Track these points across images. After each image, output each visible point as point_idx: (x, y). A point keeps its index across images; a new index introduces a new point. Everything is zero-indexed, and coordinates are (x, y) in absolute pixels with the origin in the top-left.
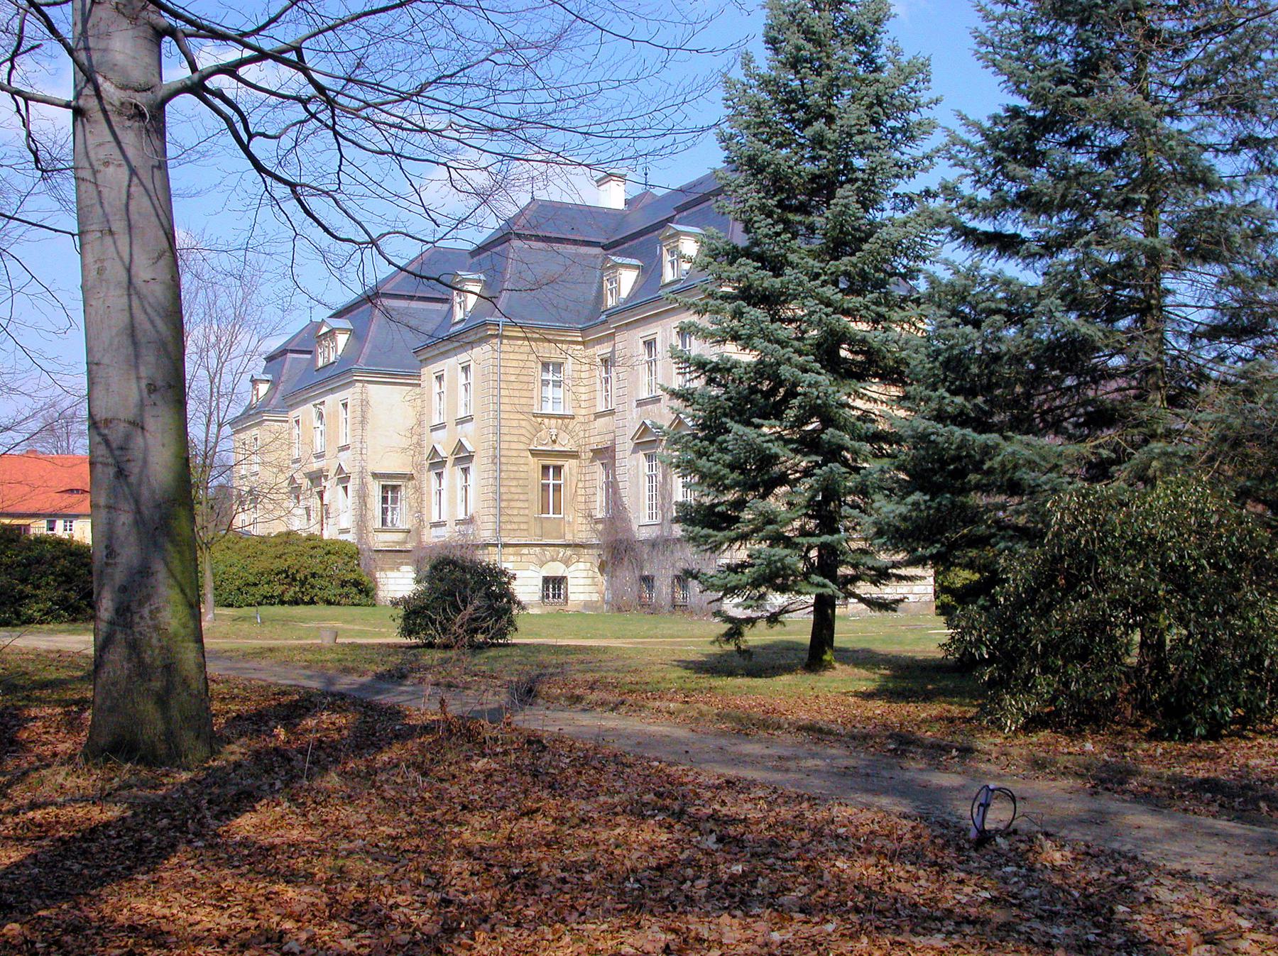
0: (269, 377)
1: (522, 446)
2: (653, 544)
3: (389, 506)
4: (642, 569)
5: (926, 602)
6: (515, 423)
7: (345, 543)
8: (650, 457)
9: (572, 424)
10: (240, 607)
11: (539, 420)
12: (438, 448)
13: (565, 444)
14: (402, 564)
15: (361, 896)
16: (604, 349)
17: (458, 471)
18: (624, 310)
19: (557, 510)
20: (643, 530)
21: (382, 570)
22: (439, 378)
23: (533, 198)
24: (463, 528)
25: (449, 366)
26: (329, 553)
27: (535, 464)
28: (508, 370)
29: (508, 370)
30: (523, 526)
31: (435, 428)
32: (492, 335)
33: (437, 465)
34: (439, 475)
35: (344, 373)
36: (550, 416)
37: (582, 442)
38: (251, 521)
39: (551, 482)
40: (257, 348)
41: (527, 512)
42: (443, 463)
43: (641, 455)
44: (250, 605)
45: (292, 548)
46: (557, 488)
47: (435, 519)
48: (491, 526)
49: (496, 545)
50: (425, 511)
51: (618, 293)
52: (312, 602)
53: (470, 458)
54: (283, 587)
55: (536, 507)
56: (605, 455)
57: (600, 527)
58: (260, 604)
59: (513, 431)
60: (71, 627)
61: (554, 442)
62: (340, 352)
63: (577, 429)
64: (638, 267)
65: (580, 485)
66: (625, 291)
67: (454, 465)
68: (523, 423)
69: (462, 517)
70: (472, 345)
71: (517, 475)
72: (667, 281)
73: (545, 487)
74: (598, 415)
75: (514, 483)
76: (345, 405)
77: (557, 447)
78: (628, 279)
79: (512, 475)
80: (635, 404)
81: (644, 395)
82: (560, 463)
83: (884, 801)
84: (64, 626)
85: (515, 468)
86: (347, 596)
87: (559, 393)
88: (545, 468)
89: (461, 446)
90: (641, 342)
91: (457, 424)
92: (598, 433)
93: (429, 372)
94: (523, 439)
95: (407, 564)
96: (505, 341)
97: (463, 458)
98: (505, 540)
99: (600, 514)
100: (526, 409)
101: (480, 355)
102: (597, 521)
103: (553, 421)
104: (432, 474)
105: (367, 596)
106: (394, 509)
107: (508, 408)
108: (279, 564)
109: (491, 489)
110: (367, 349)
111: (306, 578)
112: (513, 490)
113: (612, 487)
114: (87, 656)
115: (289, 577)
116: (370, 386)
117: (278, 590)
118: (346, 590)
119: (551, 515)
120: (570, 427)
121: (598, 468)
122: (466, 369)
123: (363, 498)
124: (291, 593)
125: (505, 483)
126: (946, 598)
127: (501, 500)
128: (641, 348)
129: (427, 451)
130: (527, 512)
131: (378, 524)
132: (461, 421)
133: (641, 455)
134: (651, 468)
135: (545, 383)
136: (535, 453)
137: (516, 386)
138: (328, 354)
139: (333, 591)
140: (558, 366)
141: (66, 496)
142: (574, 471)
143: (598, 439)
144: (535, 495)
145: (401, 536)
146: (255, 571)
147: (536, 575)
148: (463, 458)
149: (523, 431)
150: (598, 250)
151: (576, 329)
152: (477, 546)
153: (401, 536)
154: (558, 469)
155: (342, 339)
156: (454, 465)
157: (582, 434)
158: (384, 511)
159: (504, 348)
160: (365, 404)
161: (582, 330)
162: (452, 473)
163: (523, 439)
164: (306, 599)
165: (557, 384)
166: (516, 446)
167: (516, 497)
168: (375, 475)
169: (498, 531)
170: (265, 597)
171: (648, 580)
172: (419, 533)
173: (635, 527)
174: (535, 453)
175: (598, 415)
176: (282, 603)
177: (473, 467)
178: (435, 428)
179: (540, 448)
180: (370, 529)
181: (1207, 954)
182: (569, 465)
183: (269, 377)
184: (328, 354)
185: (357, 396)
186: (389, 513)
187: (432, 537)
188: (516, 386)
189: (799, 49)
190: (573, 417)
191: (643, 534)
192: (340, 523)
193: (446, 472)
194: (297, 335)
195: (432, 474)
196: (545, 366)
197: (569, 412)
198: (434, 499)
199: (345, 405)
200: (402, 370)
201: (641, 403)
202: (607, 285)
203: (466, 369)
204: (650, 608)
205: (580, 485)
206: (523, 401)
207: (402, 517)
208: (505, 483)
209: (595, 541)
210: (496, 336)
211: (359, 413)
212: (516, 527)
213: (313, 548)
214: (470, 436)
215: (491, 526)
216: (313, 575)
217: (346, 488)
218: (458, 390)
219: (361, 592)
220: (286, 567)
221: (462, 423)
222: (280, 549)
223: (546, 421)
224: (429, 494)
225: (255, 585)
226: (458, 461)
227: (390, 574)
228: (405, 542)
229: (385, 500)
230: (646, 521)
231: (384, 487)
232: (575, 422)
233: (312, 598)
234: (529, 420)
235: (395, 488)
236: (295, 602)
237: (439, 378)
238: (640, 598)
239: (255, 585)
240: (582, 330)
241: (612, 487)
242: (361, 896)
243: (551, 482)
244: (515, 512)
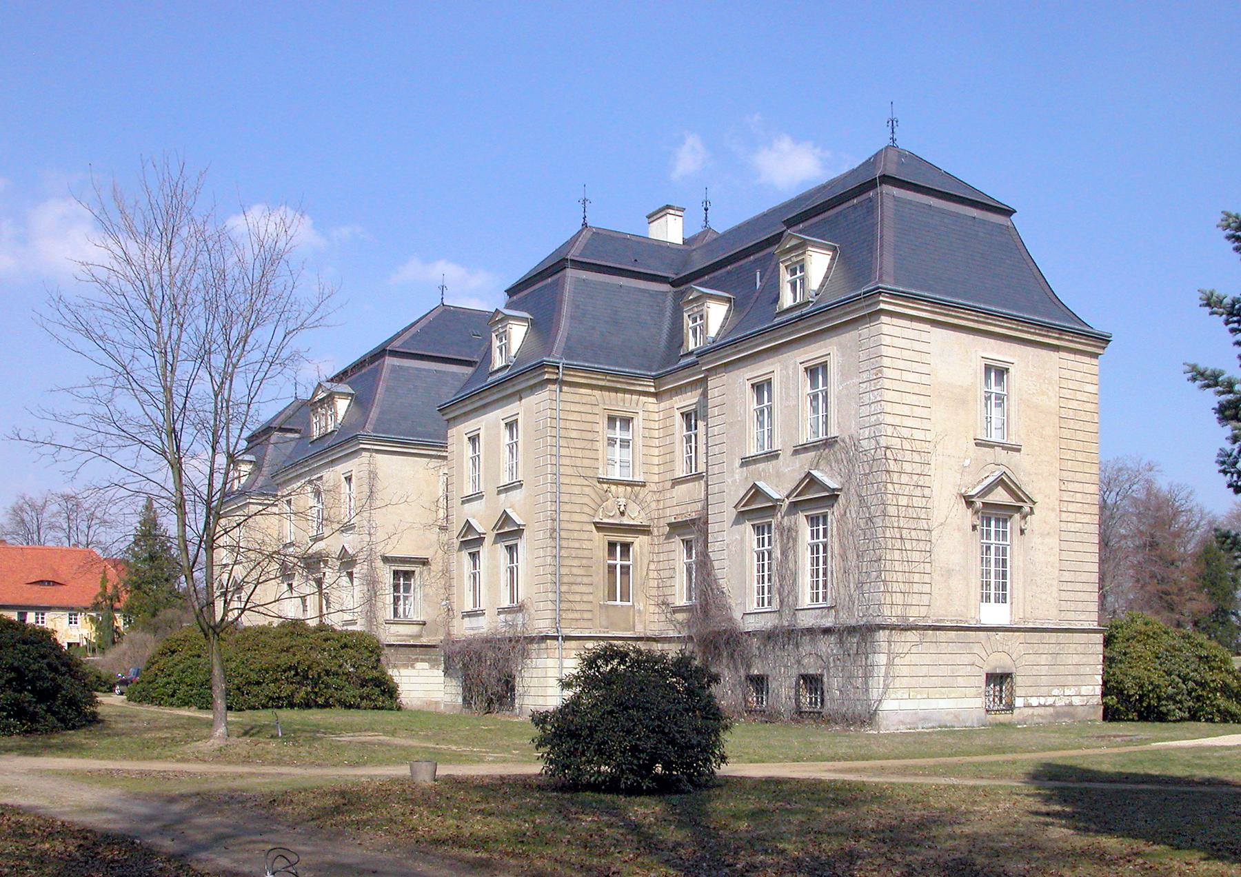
0: (252, 458)
1: (586, 518)
2: (769, 636)
3: (402, 594)
4: (749, 667)
5: (1093, 706)
6: (576, 490)
7: (353, 633)
8: (759, 529)
9: (643, 492)
10: (240, 710)
11: (605, 486)
12: (473, 522)
13: (635, 516)
14: (417, 660)
16: (689, 400)
17: (501, 549)
18: (723, 346)
19: (625, 596)
20: (751, 619)
21: (395, 666)
22: (474, 440)
23: (585, 225)
24: (509, 617)
25: (490, 423)
26: (345, 646)
27: (600, 540)
28: (568, 424)
29: (568, 424)
31: (468, 500)
32: (549, 381)
33: (471, 542)
34: (474, 556)
35: (347, 441)
36: (617, 483)
37: (655, 515)
39: (618, 562)
40: (280, 348)
41: (591, 598)
42: (480, 541)
43: (748, 527)
44: (253, 708)
45: (300, 640)
46: (625, 570)
47: (469, 607)
48: (549, 614)
49: (556, 638)
50: (455, 598)
51: (704, 330)
52: (326, 705)
53: (518, 532)
54: (293, 687)
55: (602, 590)
56: (693, 530)
57: (680, 617)
58: (265, 707)
59: (574, 499)
60: (25, 742)
61: (622, 514)
62: (340, 418)
63: (648, 499)
64: (729, 300)
65: (652, 566)
66: (714, 328)
67: (495, 542)
68: (587, 490)
69: (506, 603)
70: (519, 395)
72: (786, 306)
73: (612, 569)
74: (676, 482)
76: (349, 479)
77: (625, 520)
78: (716, 313)
80: (738, 463)
81: (753, 451)
82: (629, 540)
84: (16, 740)
85: (577, 545)
86: (368, 697)
87: (627, 454)
88: (612, 545)
89: (506, 518)
90: (748, 384)
91: (499, 493)
92: (683, 502)
93: (458, 434)
94: (586, 509)
95: (423, 660)
96: (565, 389)
97: (509, 532)
98: (567, 632)
99: (681, 600)
100: (589, 473)
101: (531, 408)
102: (677, 610)
103: (621, 489)
104: (465, 555)
105: (391, 697)
106: (406, 598)
107: (569, 471)
108: (285, 659)
109: (550, 569)
110: (374, 414)
111: (319, 676)
112: (575, 571)
113: (702, 570)
115: (300, 675)
116: (379, 456)
117: (286, 689)
118: (366, 690)
119: (618, 602)
120: (641, 496)
121: (677, 545)
122: (511, 425)
123: (372, 582)
124: (302, 694)
125: (566, 562)
126: (1112, 700)
127: (561, 584)
128: (750, 395)
129: (457, 527)
130: (591, 598)
131: (389, 615)
132: (507, 489)
133: (748, 527)
134: (761, 543)
135: (611, 442)
136: (600, 527)
137: (578, 444)
138: (322, 424)
139: (351, 693)
140: (627, 422)
141: (36, 587)
142: (646, 549)
143: (677, 510)
144: (600, 577)
145: (415, 629)
146: (257, 666)
148: (509, 532)
149: (586, 500)
150: (665, 287)
151: (648, 377)
152: (531, 640)
153: (415, 629)
154: (626, 547)
155: (342, 405)
156: (495, 542)
157: (654, 505)
158: (396, 599)
159: (564, 397)
160: (373, 476)
161: (655, 378)
162: (493, 555)
163: (586, 509)
164: (320, 701)
165: (625, 444)
166: (578, 518)
167: (579, 580)
168: (386, 560)
169: (557, 622)
170: (271, 698)
171: (759, 682)
172: (447, 624)
173: (737, 615)
174: (600, 527)
175: (676, 482)
176: (292, 705)
177: (522, 544)
178: (468, 500)
179: (605, 520)
180: (381, 620)
182: (639, 543)
183: (252, 458)
184: (322, 424)
185: (365, 468)
186: (401, 602)
187: (464, 629)
188: (578, 444)
190: (643, 485)
191: (752, 624)
192: (346, 607)
193: (484, 551)
194: (280, 413)
195: (465, 555)
196: (612, 420)
197: (639, 478)
198: (468, 583)
199: (349, 479)
200: (423, 437)
201: (746, 462)
202: (688, 323)
203: (511, 425)
204: (770, 717)
205: (652, 566)
206: (586, 463)
207: (418, 606)
208: (566, 562)
209: (671, 634)
210: (554, 381)
211: (366, 488)
212: (577, 615)
213: (326, 640)
214: (517, 506)
215: (549, 614)
216: (328, 673)
217: (350, 575)
218: (501, 451)
219: (383, 692)
220: (295, 662)
221: (468, 501)
222: (287, 641)
223: (613, 488)
224: (461, 576)
225: (258, 683)
226: (500, 537)
227: (404, 671)
228: (420, 636)
229: (396, 588)
230: (753, 607)
231: (396, 573)
232: (646, 490)
233: (327, 701)
234: (593, 487)
235: (408, 575)
236: (307, 705)
237: (474, 440)
238: (746, 701)
239: (258, 683)
240: (655, 378)
241: (702, 570)
243: (618, 562)
244: (578, 598)
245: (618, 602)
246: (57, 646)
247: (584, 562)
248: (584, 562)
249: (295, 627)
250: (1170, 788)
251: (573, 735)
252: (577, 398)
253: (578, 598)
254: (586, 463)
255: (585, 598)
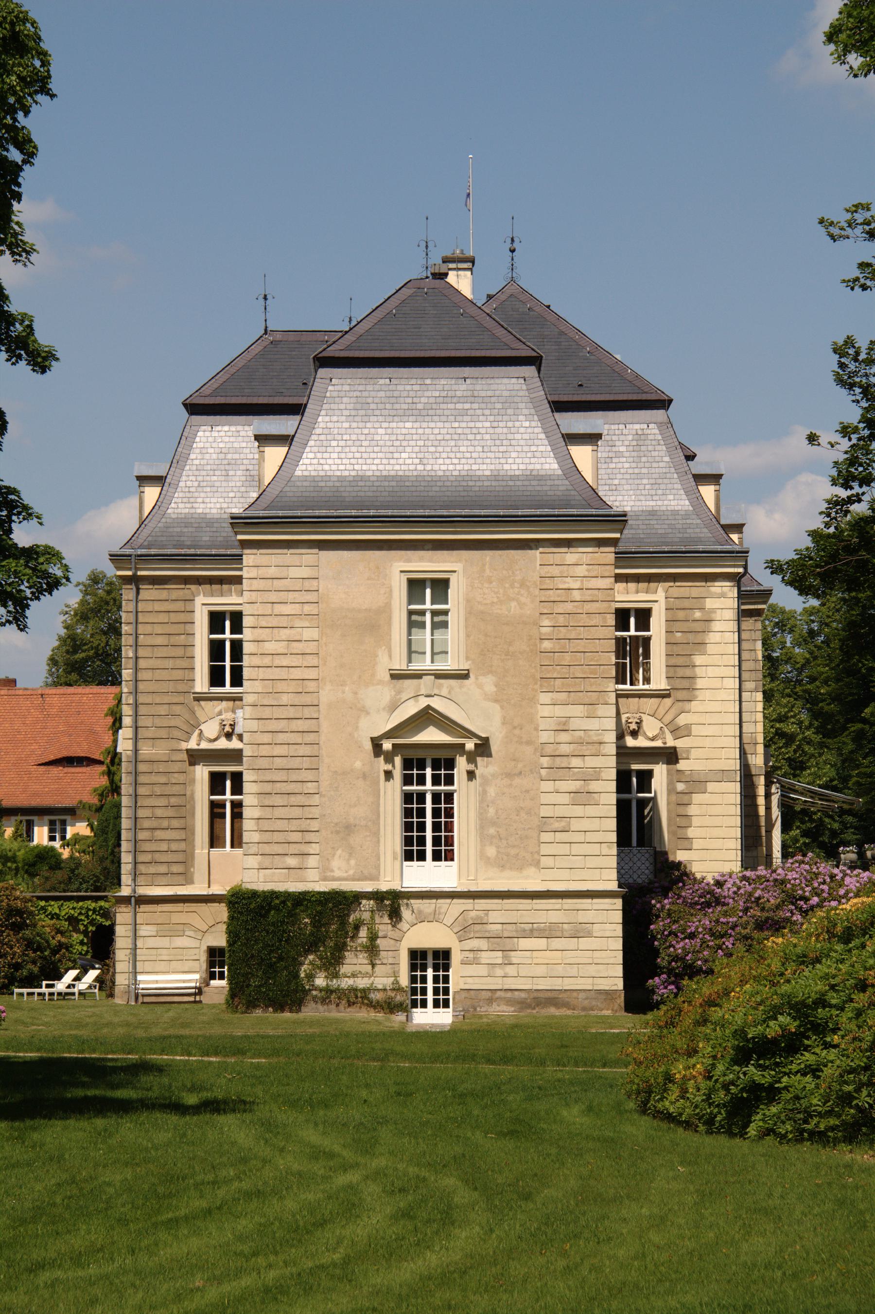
6: (163, 710)
15: (543, 1113)
19: (237, 680)
30: (175, 869)
38: (224, 905)
39: (228, 635)
68: (177, 709)
71: (168, 790)
75: (162, 802)
79: (158, 790)
83: (443, 382)
85: (162, 779)
100: (181, 687)
112: (159, 812)
114: (608, 994)
119: (228, 688)
137: (163, 652)
147: (195, 943)
167: (165, 824)
181: (874, 1018)
188: (163, 652)
189: (837, 1283)
206: (178, 674)
242: (543, 1113)
244: (164, 846)
245: (228, 688)
246: (667, 859)
247: (173, 801)
248: (173, 801)
249: (645, 1014)
250: (93, 1270)
251: (40, 858)
252: (164, 594)
253: (164, 846)
254: (178, 674)
255: (174, 846)
